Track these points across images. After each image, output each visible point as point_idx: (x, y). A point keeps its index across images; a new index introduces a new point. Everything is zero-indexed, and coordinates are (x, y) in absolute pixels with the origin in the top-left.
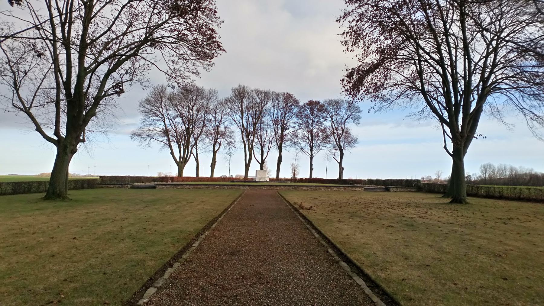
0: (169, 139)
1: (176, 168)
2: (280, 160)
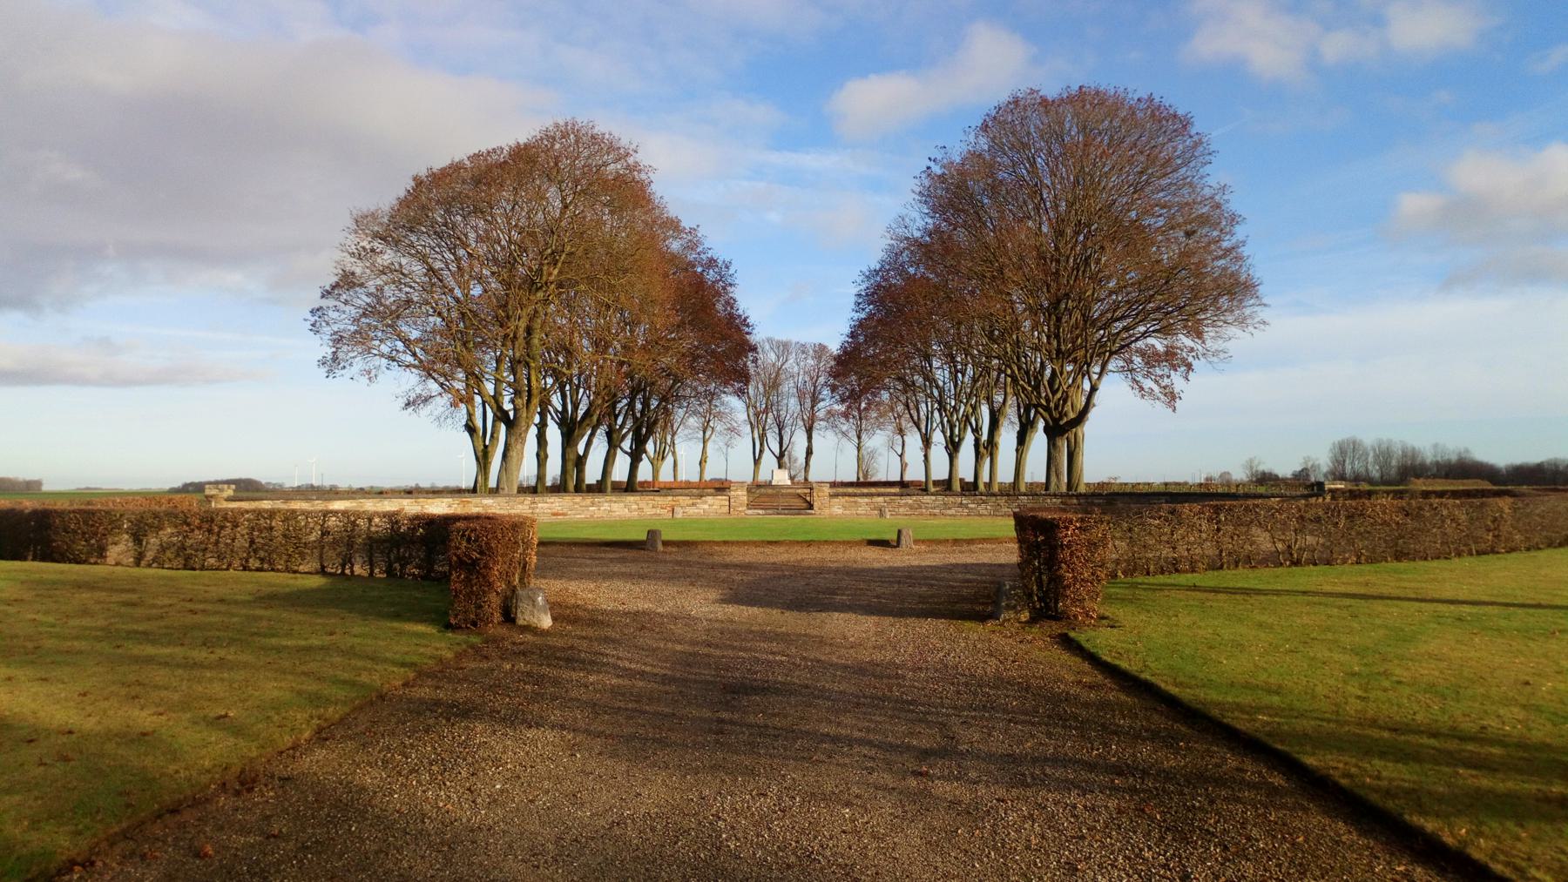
2: (809, 452)
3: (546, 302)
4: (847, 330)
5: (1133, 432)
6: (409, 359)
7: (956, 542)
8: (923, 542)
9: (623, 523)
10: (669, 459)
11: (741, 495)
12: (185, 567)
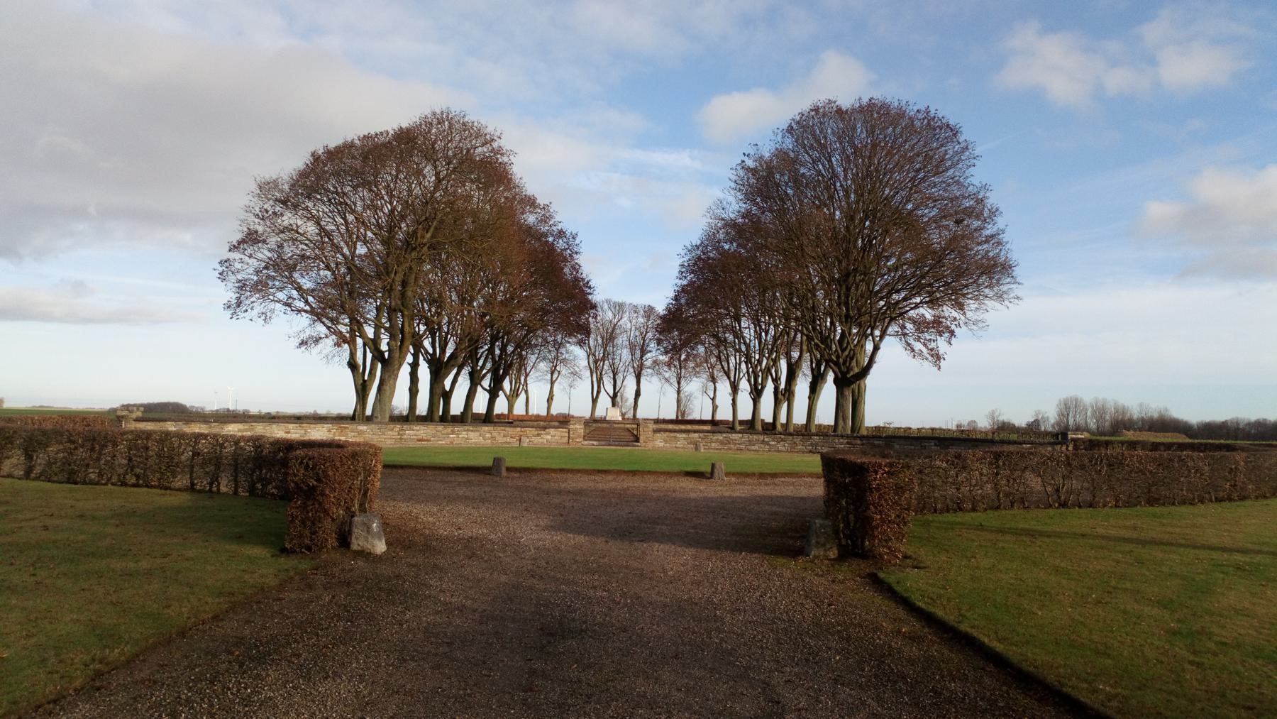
2: (638, 394)
3: (420, 261)
4: (672, 294)
5: (910, 386)
6: (301, 304)
7: (762, 475)
8: (734, 474)
9: (477, 450)
10: (523, 396)
11: (579, 429)
12: (68, 482)
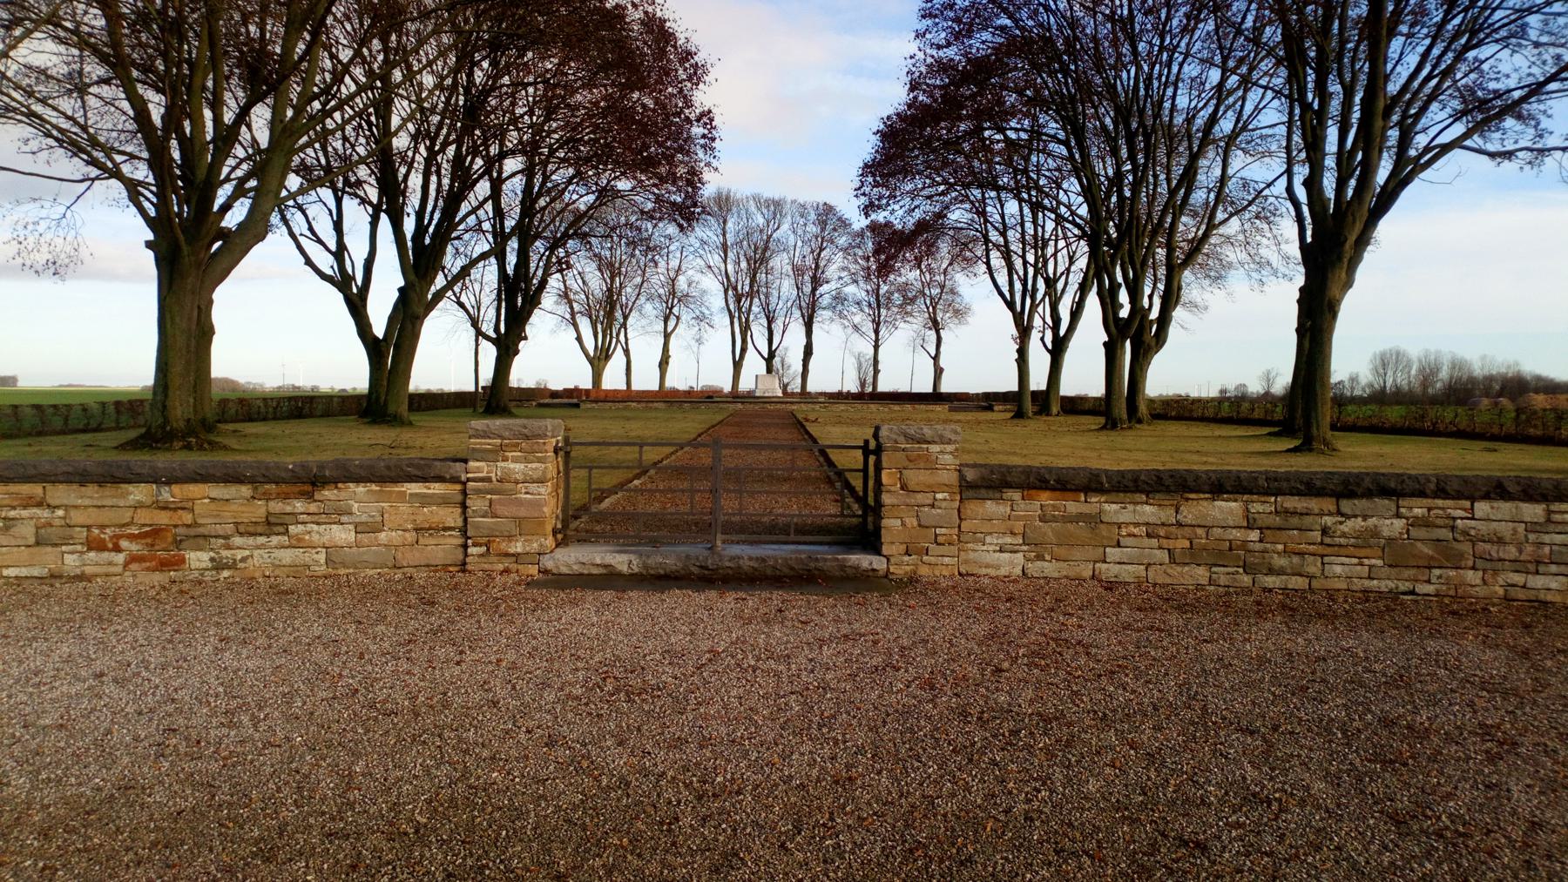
0: (572, 308)
1: (587, 370)
2: (808, 351)
